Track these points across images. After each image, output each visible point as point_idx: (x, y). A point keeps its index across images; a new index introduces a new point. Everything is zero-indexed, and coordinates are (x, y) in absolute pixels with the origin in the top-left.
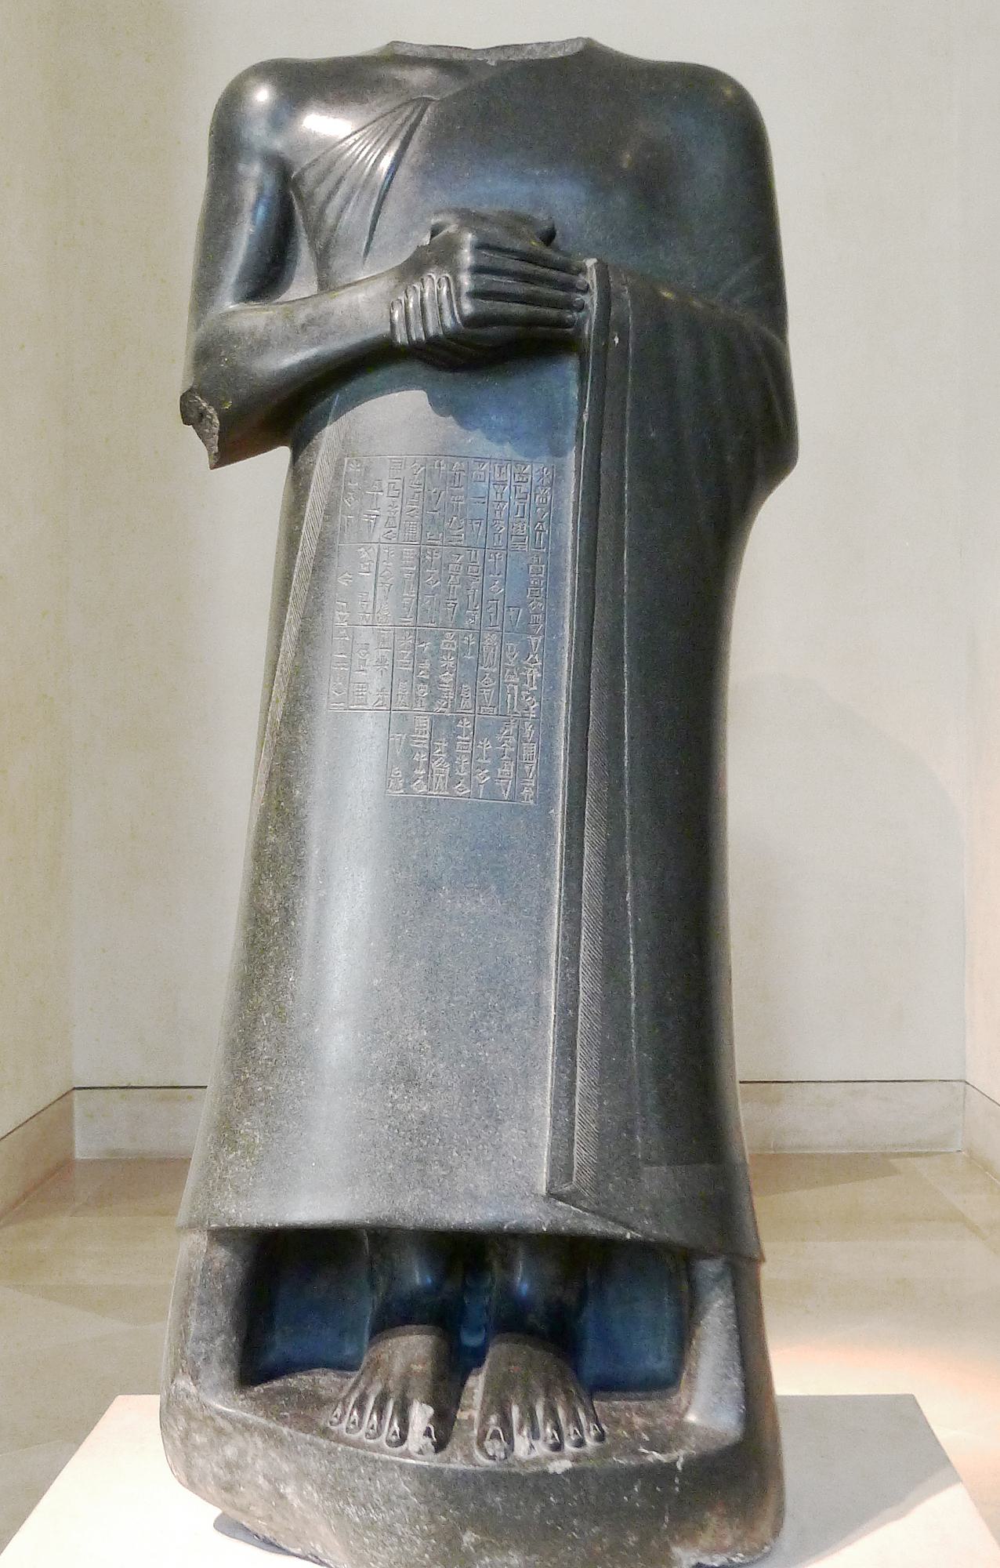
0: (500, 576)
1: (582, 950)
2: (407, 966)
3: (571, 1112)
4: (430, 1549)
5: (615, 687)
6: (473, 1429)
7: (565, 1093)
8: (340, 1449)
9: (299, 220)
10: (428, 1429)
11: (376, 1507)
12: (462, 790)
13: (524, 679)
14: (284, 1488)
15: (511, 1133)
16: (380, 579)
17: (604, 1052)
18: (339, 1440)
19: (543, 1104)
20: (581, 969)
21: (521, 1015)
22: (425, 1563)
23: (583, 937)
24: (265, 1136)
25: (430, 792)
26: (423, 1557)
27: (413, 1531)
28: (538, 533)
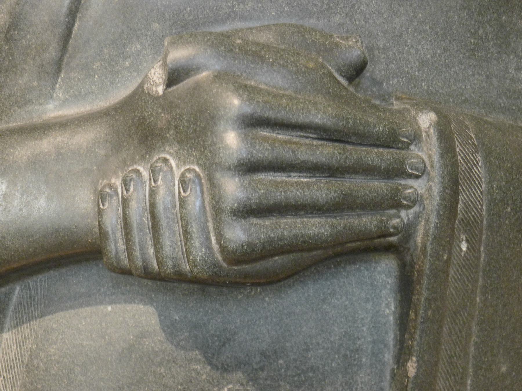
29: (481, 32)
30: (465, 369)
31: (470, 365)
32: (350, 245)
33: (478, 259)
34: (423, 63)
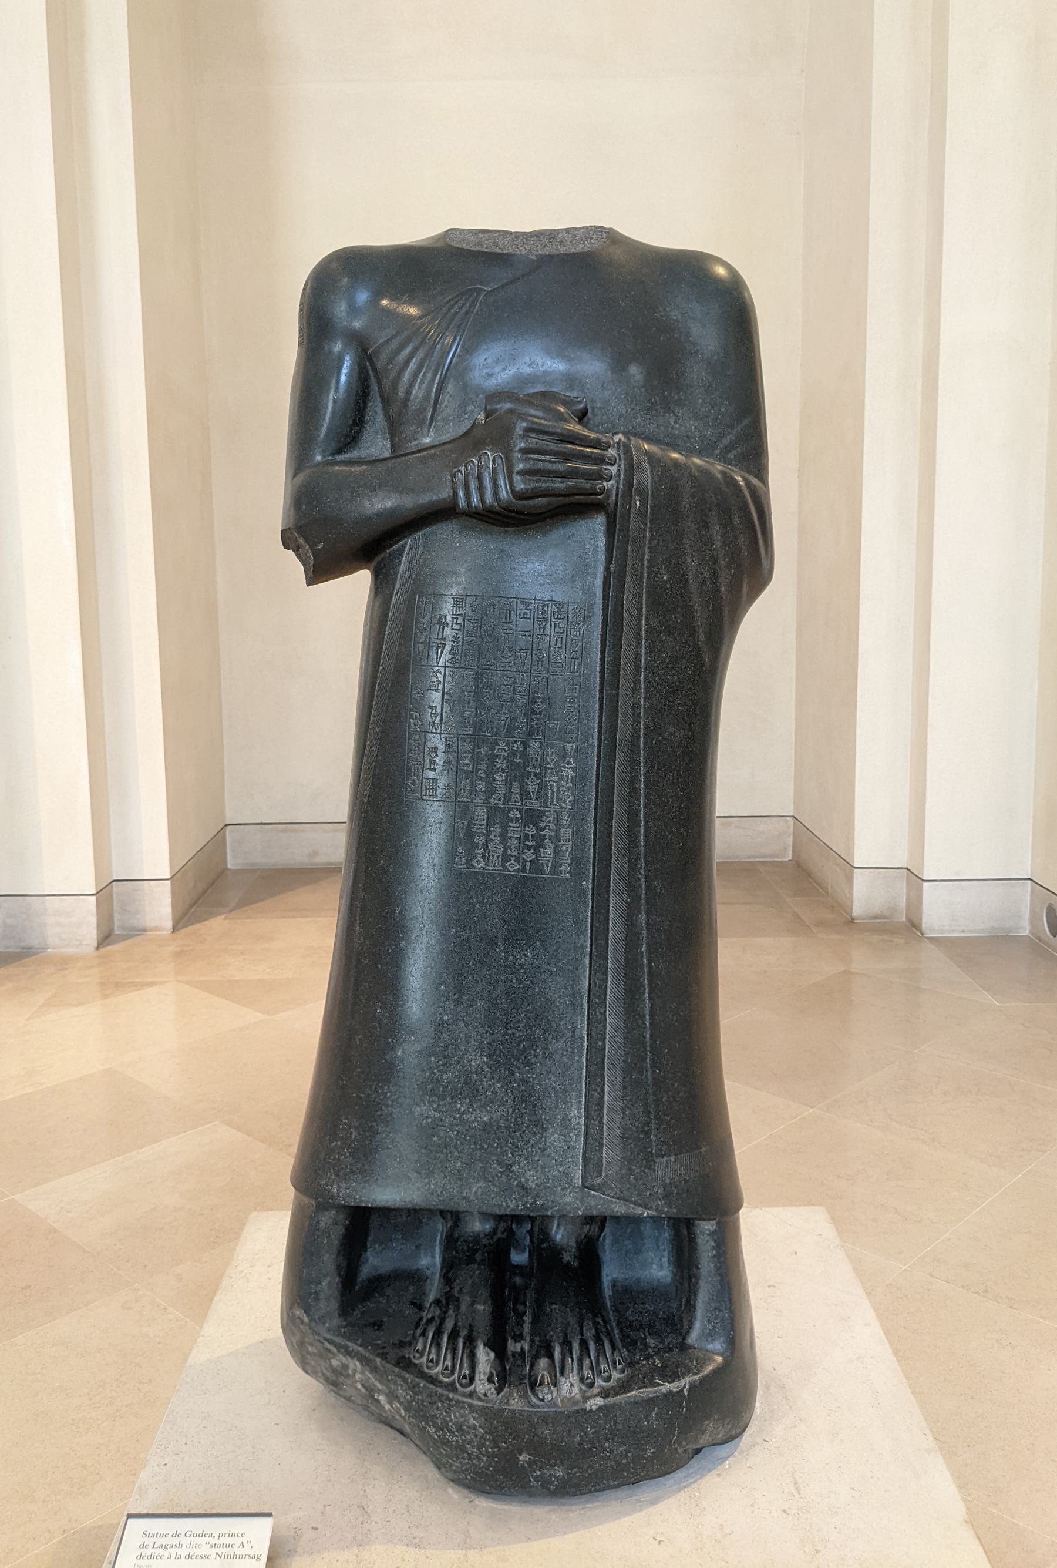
0: (543, 695)
1: (608, 993)
2: (470, 1006)
3: (601, 1122)
4: (493, 1464)
5: (633, 781)
6: (526, 1366)
7: (593, 1109)
8: (422, 1385)
9: (374, 387)
10: (491, 1374)
11: (451, 1432)
12: (513, 867)
13: (561, 778)
14: (378, 1396)
15: (553, 1137)
16: (445, 697)
17: (627, 1072)
18: (422, 1375)
19: (576, 1114)
20: (608, 1008)
21: (561, 1044)
22: (489, 1473)
23: (609, 983)
24: (359, 1134)
25: (488, 868)
26: (488, 1469)
27: (480, 1451)
28: (573, 660)
29: (653, 400)
30: (642, 573)
31: (645, 572)
32: (577, 497)
33: (647, 511)
34: (621, 416)
